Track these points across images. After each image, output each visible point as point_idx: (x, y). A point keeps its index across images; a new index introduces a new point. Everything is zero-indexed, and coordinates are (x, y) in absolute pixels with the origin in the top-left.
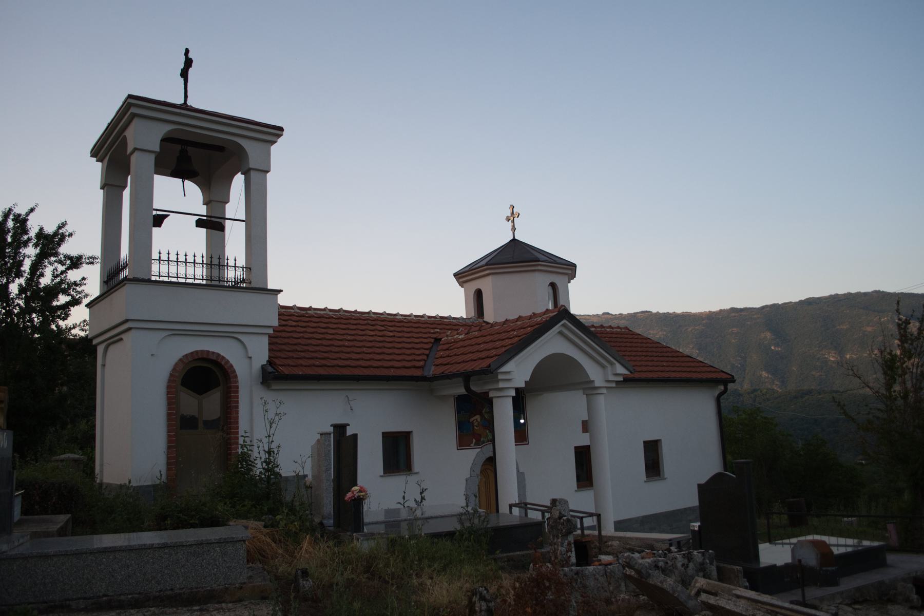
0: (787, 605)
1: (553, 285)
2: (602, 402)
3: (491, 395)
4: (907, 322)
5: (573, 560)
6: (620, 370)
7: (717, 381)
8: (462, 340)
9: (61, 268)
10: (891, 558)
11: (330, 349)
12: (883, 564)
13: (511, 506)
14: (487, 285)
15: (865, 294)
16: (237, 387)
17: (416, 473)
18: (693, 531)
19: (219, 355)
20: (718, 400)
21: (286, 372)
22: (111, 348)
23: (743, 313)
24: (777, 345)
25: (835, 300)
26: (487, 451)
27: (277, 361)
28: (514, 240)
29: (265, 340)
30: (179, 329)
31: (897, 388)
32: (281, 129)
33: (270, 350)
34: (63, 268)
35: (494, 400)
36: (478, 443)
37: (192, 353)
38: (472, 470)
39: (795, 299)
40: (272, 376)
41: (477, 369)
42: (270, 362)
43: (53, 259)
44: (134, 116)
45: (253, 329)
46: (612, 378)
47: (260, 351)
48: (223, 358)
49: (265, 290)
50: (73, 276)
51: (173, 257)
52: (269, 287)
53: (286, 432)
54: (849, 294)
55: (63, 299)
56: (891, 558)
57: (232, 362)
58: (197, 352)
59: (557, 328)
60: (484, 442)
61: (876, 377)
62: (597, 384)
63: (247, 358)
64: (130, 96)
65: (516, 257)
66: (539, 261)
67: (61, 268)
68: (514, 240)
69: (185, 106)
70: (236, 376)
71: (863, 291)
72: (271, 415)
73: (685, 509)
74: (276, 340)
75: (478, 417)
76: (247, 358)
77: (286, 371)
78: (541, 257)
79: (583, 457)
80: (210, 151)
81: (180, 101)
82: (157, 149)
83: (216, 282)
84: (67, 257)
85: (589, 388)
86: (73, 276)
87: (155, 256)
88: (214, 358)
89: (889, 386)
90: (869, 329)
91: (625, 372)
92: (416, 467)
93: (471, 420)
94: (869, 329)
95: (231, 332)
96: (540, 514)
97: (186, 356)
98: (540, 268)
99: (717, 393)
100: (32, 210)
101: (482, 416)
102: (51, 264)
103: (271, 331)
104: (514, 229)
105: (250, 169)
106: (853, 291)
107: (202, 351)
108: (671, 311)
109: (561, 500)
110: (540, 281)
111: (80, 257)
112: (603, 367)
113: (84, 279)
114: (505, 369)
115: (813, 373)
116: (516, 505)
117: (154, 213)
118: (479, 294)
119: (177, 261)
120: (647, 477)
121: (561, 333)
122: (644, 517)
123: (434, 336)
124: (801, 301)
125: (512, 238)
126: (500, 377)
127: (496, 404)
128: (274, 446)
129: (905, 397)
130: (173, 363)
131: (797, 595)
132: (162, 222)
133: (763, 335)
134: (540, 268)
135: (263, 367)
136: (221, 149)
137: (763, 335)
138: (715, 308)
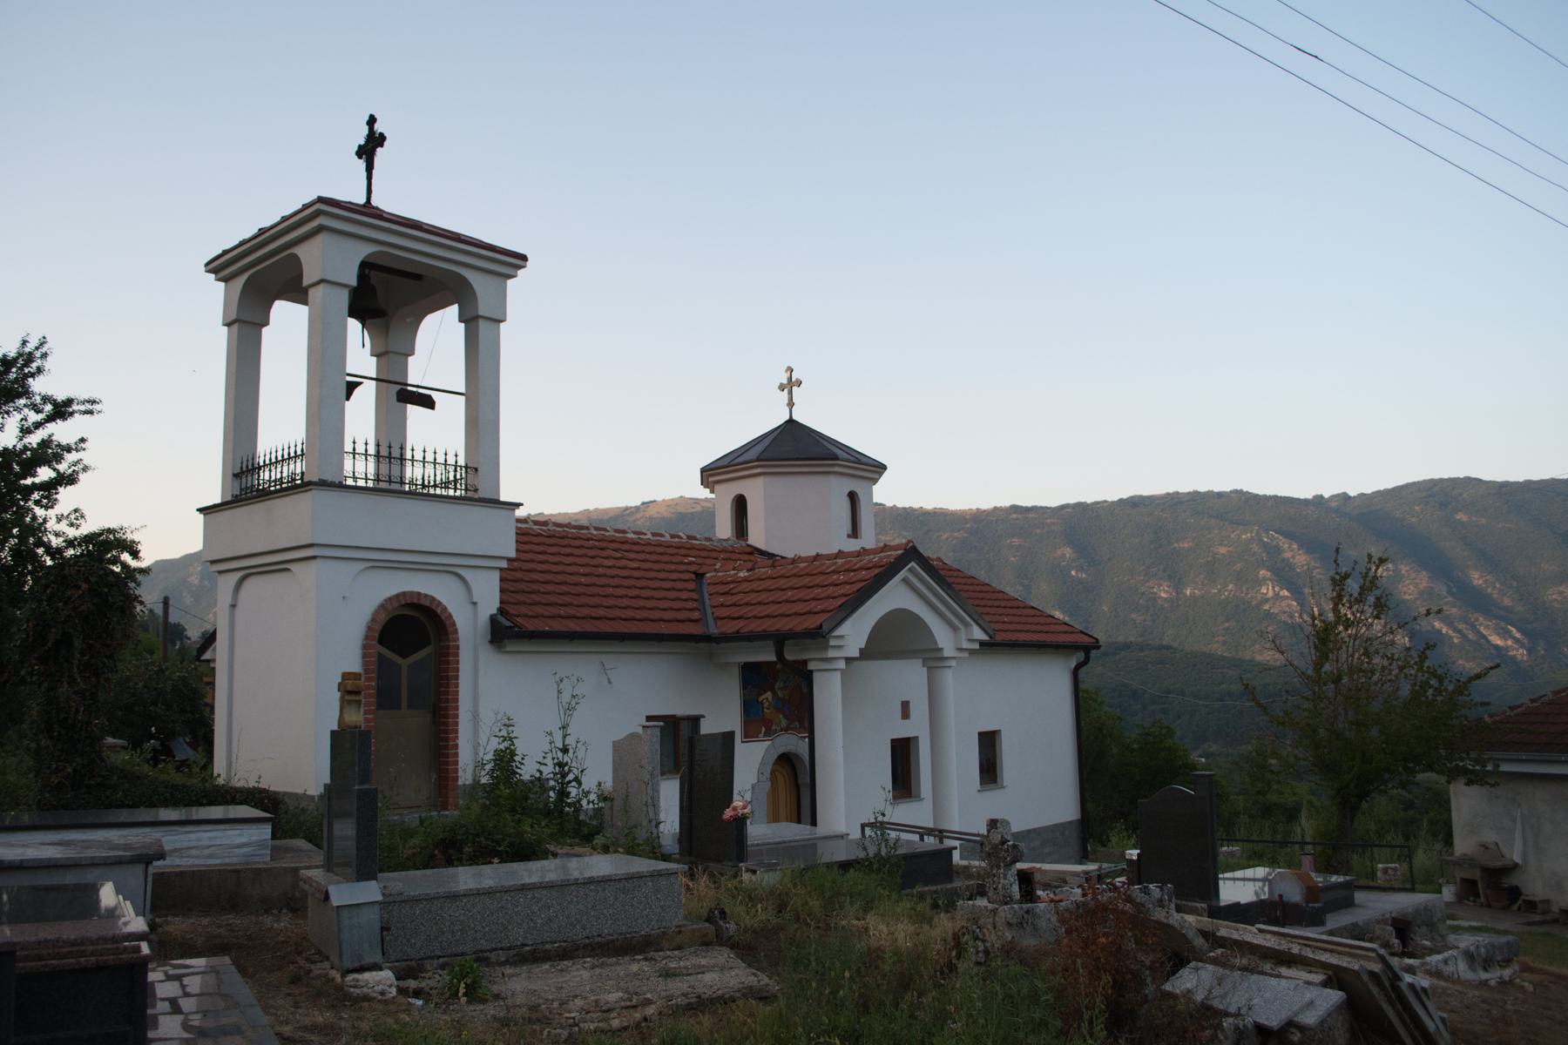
0: (1324, 937)
1: (852, 496)
2: (950, 680)
3: (811, 666)
4: (1347, 576)
5: (1018, 896)
6: (979, 634)
7: (1079, 649)
8: (745, 580)
9: (34, 417)
10: (1359, 896)
12: (1348, 903)
13: (863, 826)
14: (756, 490)
15: (1220, 495)
16: (458, 647)
18: (1131, 861)
19: (433, 599)
20: (1075, 673)
21: (531, 628)
22: (251, 584)
23: (1031, 515)
24: (1080, 569)
25: (1173, 502)
26: (793, 743)
27: (511, 609)
28: (791, 421)
29: (495, 577)
30: (383, 560)
31: (1327, 667)
32: (524, 258)
33: (502, 591)
34: (40, 417)
35: (816, 676)
37: (397, 596)
38: (760, 773)
39: (1113, 497)
40: (503, 633)
41: (798, 629)
42: (501, 611)
43: (22, 401)
45: (479, 561)
46: (966, 645)
47: (488, 593)
48: (440, 603)
49: (495, 502)
50: (61, 432)
52: (502, 499)
53: (531, 713)
54: (1196, 493)
55: (45, 474)
56: (1359, 896)
58: (404, 593)
59: (903, 573)
61: (1303, 655)
62: (946, 654)
63: (471, 604)
64: (320, 200)
65: (794, 449)
66: (837, 458)
67: (34, 417)
68: (791, 421)
69: (368, 209)
70: (456, 632)
71: (1216, 490)
72: (566, 697)
73: (1029, 832)
74: (513, 578)
75: (769, 695)
76: (471, 604)
77: (531, 625)
78: (839, 452)
79: (902, 751)
80: (403, 277)
81: (362, 200)
82: (354, 283)
83: (391, 479)
84: (46, 399)
85: (933, 658)
86: (61, 432)
87: (348, 447)
88: (426, 603)
89: (1318, 666)
90: (1223, 550)
91: (984, 637)
94: (1223, 550)
95: (451, 565)
96: (916, 837)
97: (390, 599)
99: (1074, 664)
101: (774, 694)
102: (18, 410)
103: (504, 564)
104: (791, 404)
105: (478, 317)
106: (1202, 490)
108: (916, 506)
109: (1003, 821)
110: (836, 488)
111: (69, 402)
112: (954, 628)
113: (83, 440)
114: (837, 632)
115: (1133, 616)
116: (870, 825)
117: (349, 379)
118: (740, 504)
119: (390, 457)
120: (982, 782)
121: (905, 580)
123: (694, 568)
124: (1121, 500)
126: (832, 642)
127: (818, 679)
128: (570, 741)
129: (1337, 680)
133: (1059, 552)
135: (493, 619)
136: (418, 277)
137: (1059, 552)
138: (986, 505)
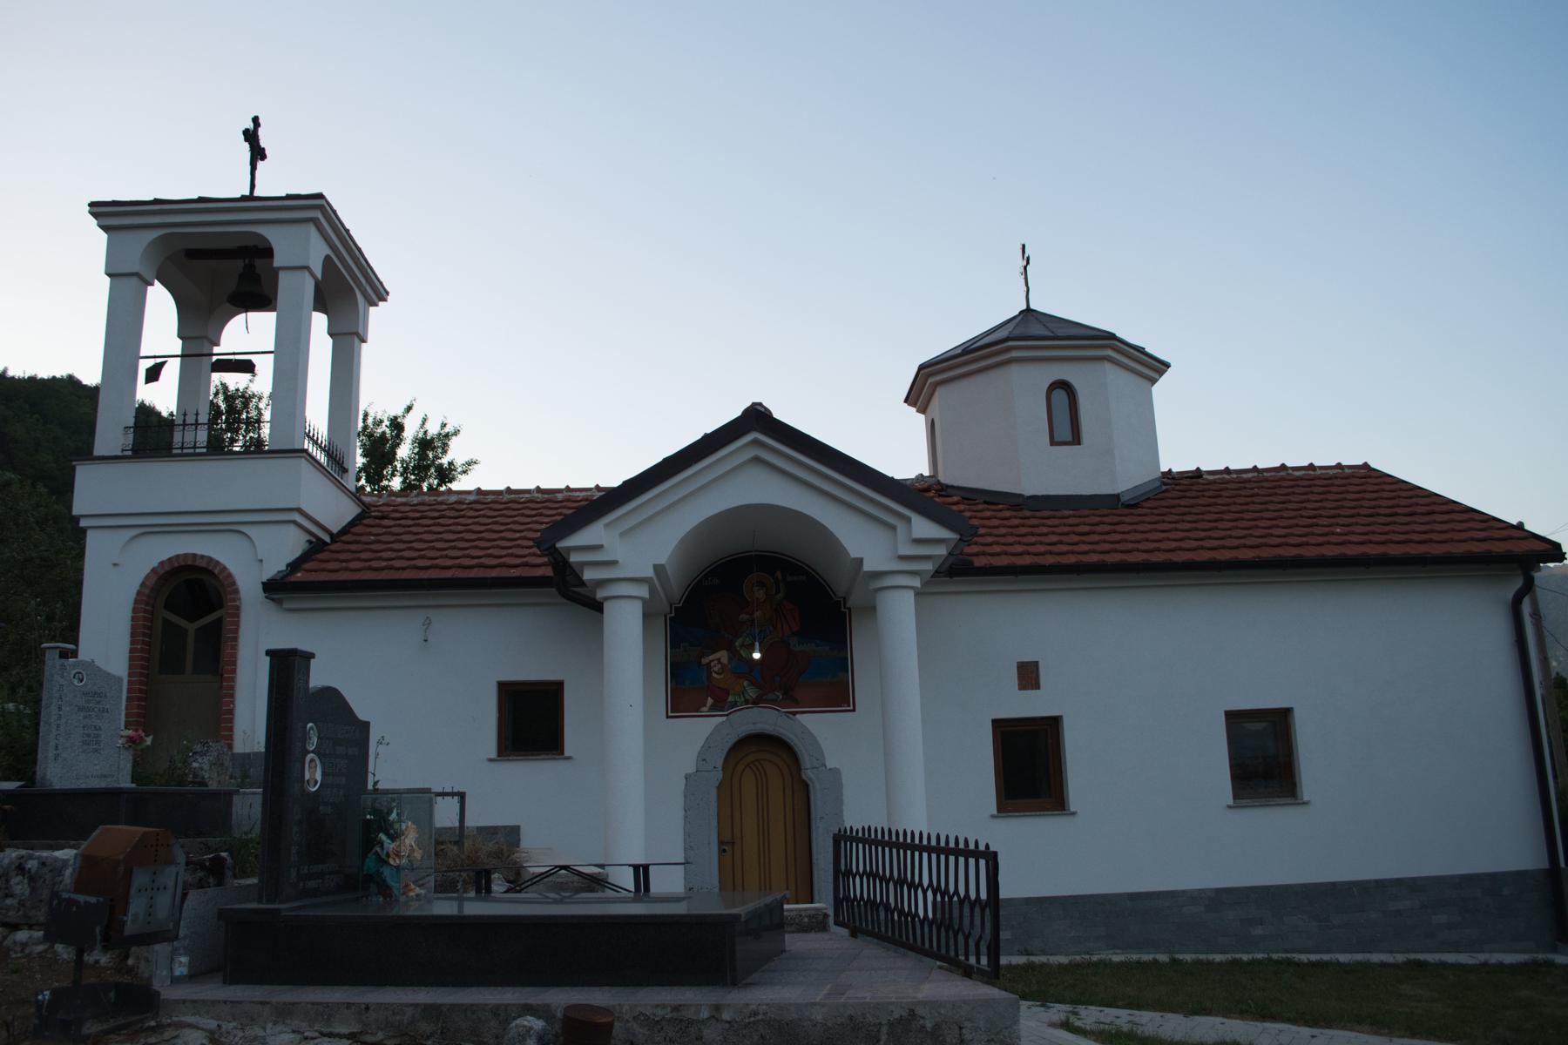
11: (424, 538)
16: (238, 608)
17: (569, 758)
19: (211, 559)
28: (1028, 312)
36: (720, 705)
38: (702, 759)
44: (315, 221)
48: (218, 563)
51: (190, 419)
57: (165, 557)
60: (735, 704)
68: (1028, 312)
70: (237, 591)
75: (723, 655)
92: (569, 749)
93: (704, 661)
95: (229, 523)
98: (1014, 354)
99: (1510, 595)
100: (409, 409)
107: (186, 555)
120: (1236, 796)
122: (1218, 891)
125: (1024, 307)
130: (143, 576)
131: (1059, 1011)
132: (746, 412)
134: (1014, 354)
